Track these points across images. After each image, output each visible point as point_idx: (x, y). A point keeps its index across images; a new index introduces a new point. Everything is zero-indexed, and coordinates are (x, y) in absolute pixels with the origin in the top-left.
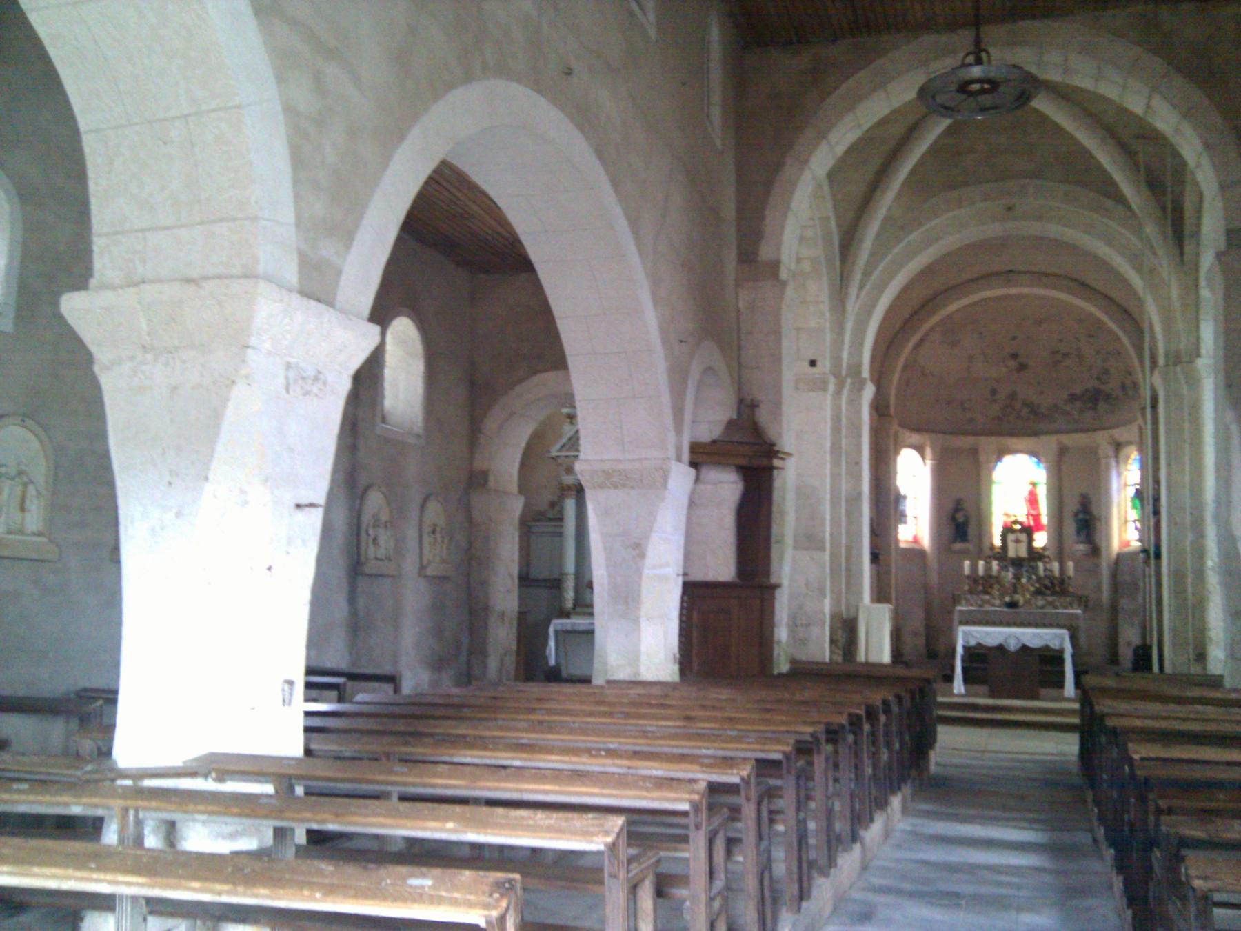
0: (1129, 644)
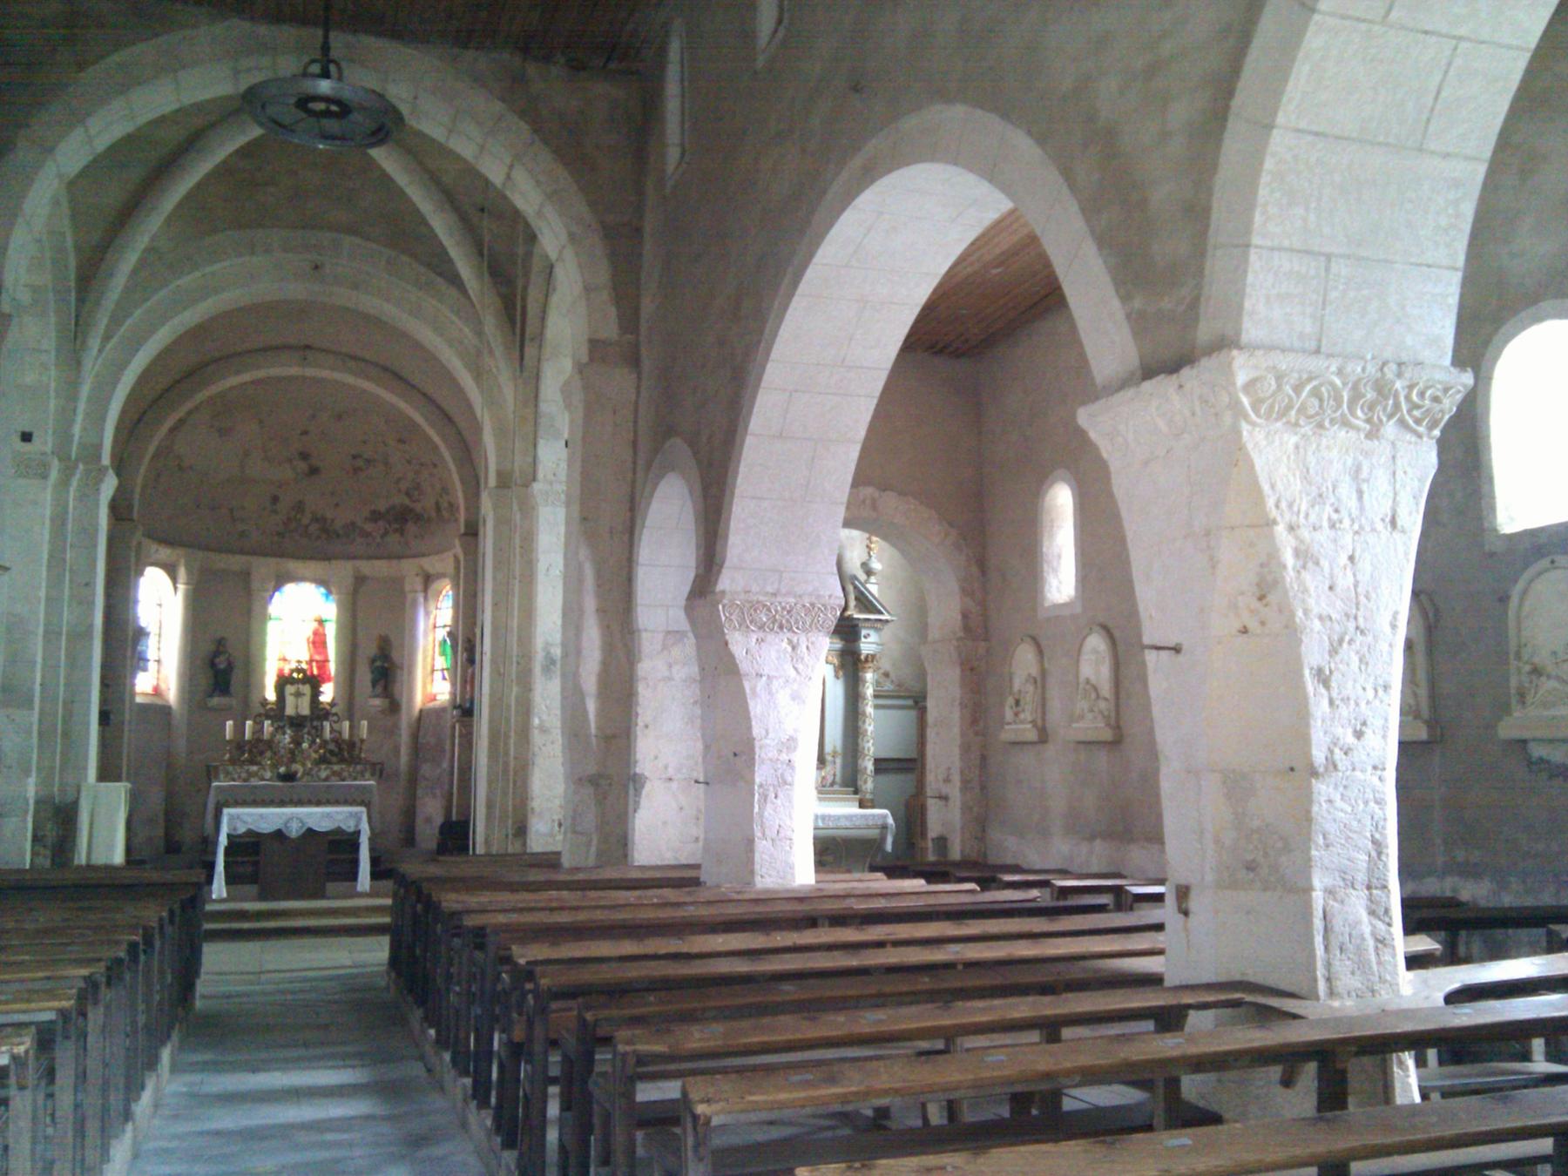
0: (428, 820)
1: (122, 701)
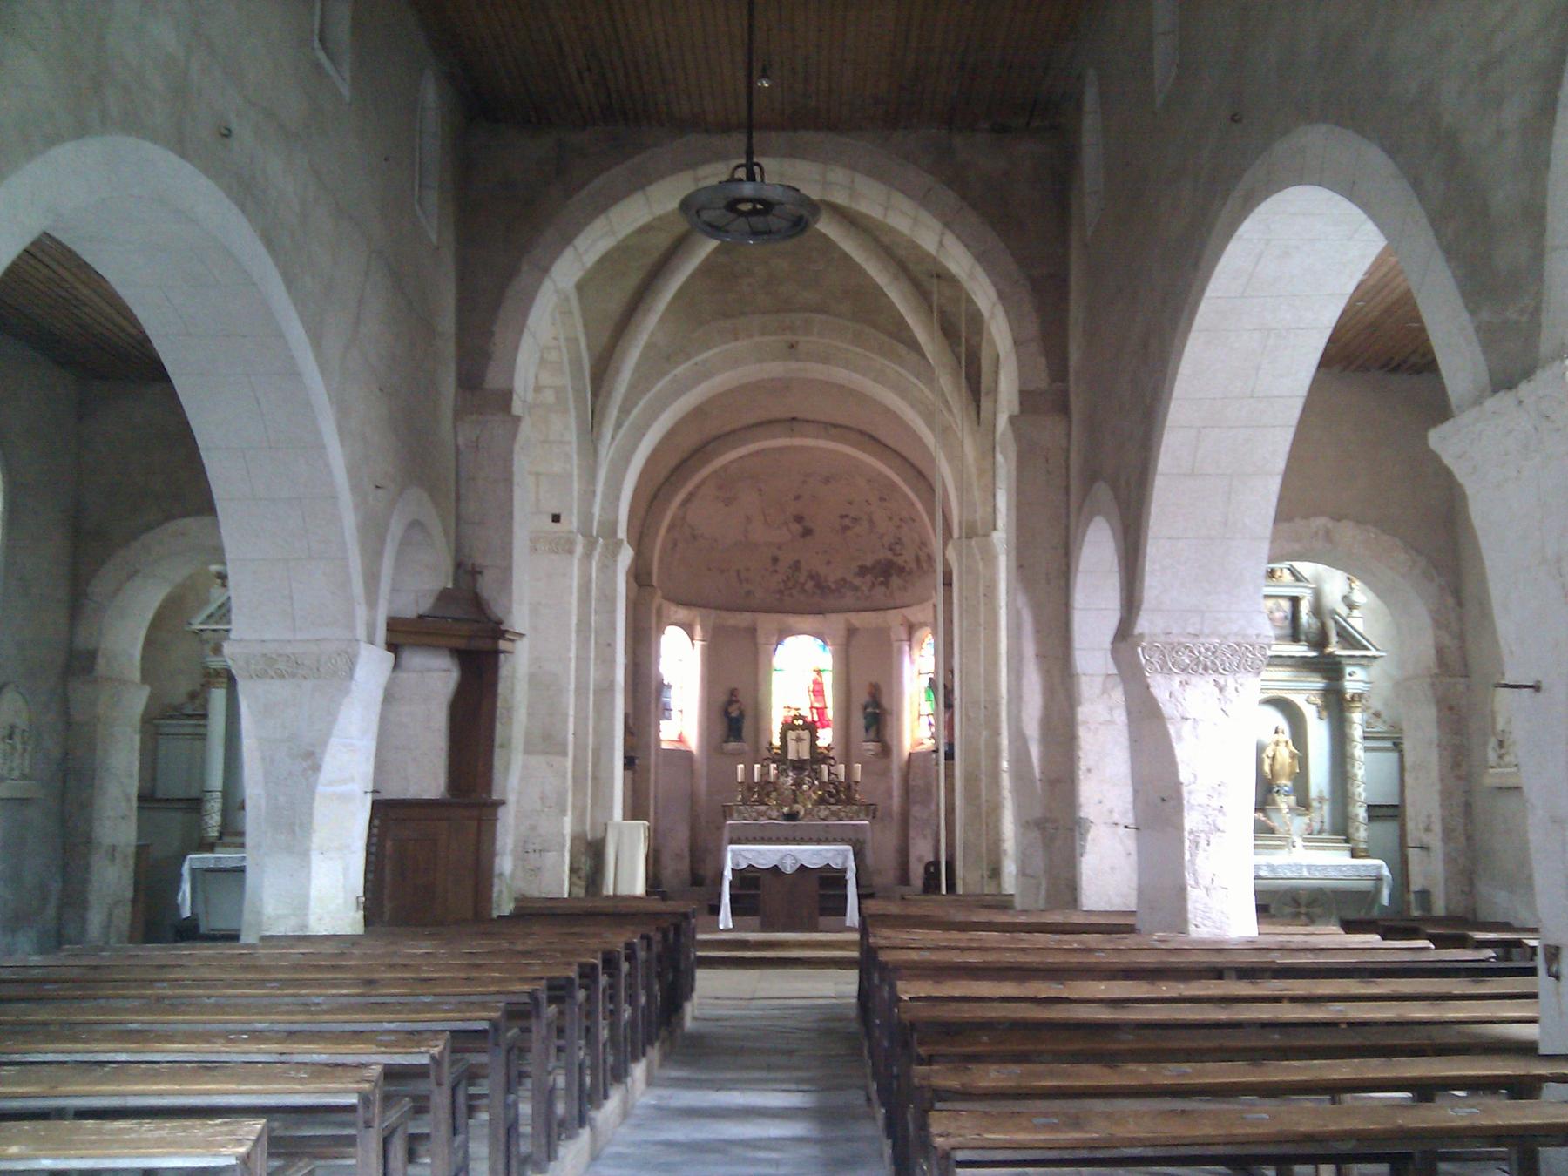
0: (920, 859)
1: (648, 746)
